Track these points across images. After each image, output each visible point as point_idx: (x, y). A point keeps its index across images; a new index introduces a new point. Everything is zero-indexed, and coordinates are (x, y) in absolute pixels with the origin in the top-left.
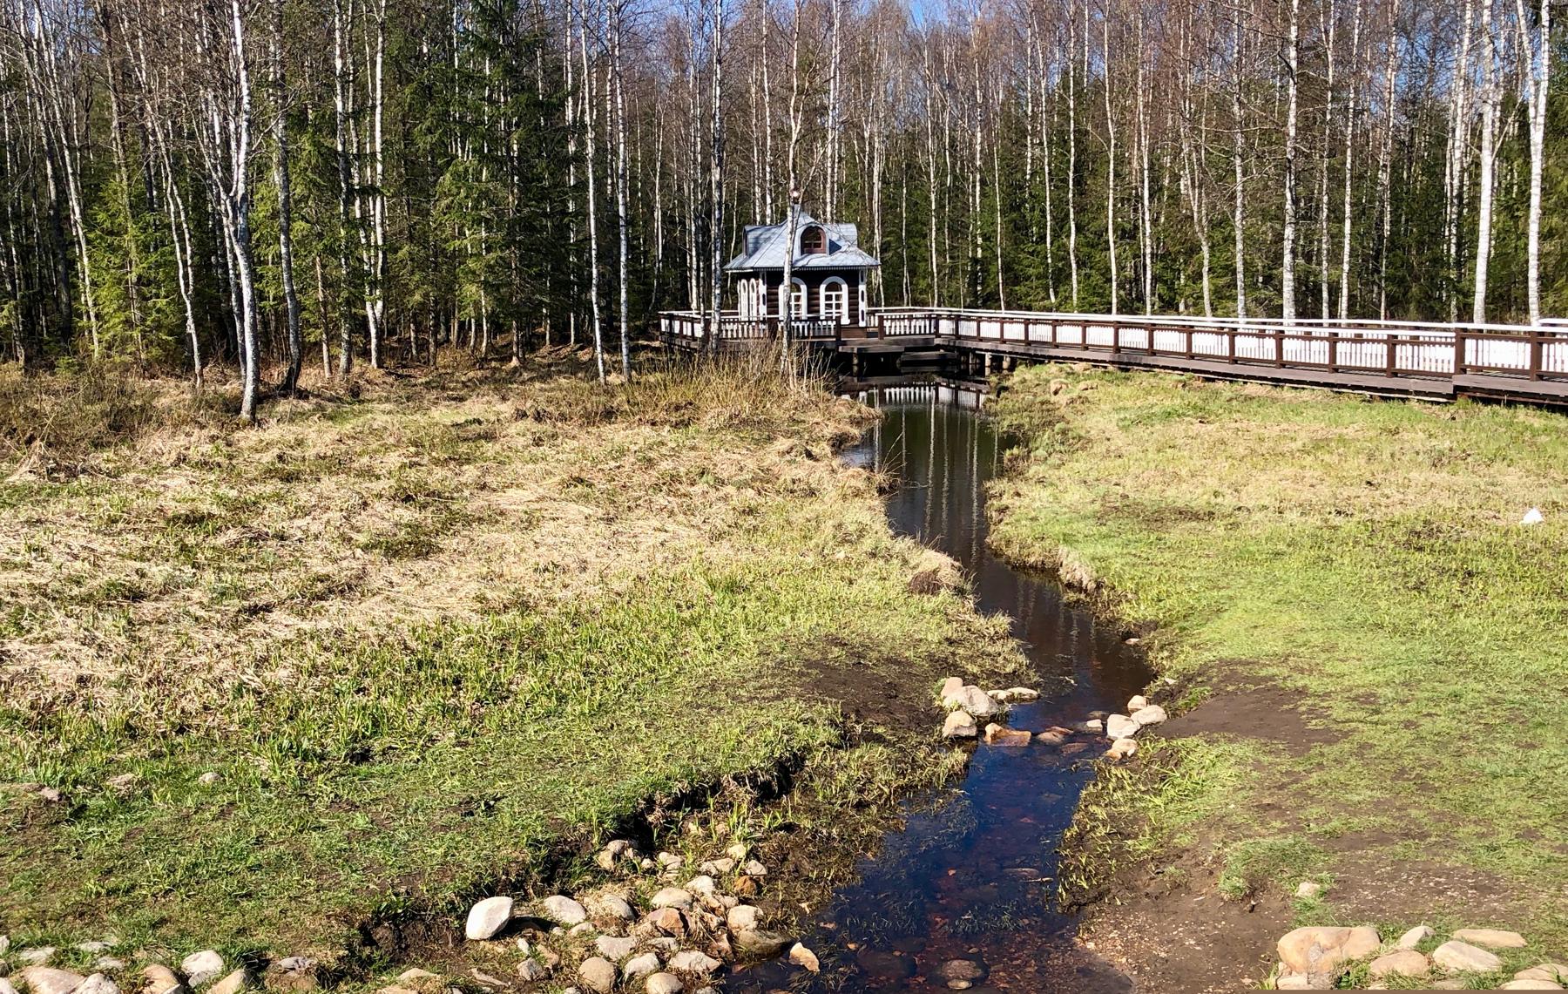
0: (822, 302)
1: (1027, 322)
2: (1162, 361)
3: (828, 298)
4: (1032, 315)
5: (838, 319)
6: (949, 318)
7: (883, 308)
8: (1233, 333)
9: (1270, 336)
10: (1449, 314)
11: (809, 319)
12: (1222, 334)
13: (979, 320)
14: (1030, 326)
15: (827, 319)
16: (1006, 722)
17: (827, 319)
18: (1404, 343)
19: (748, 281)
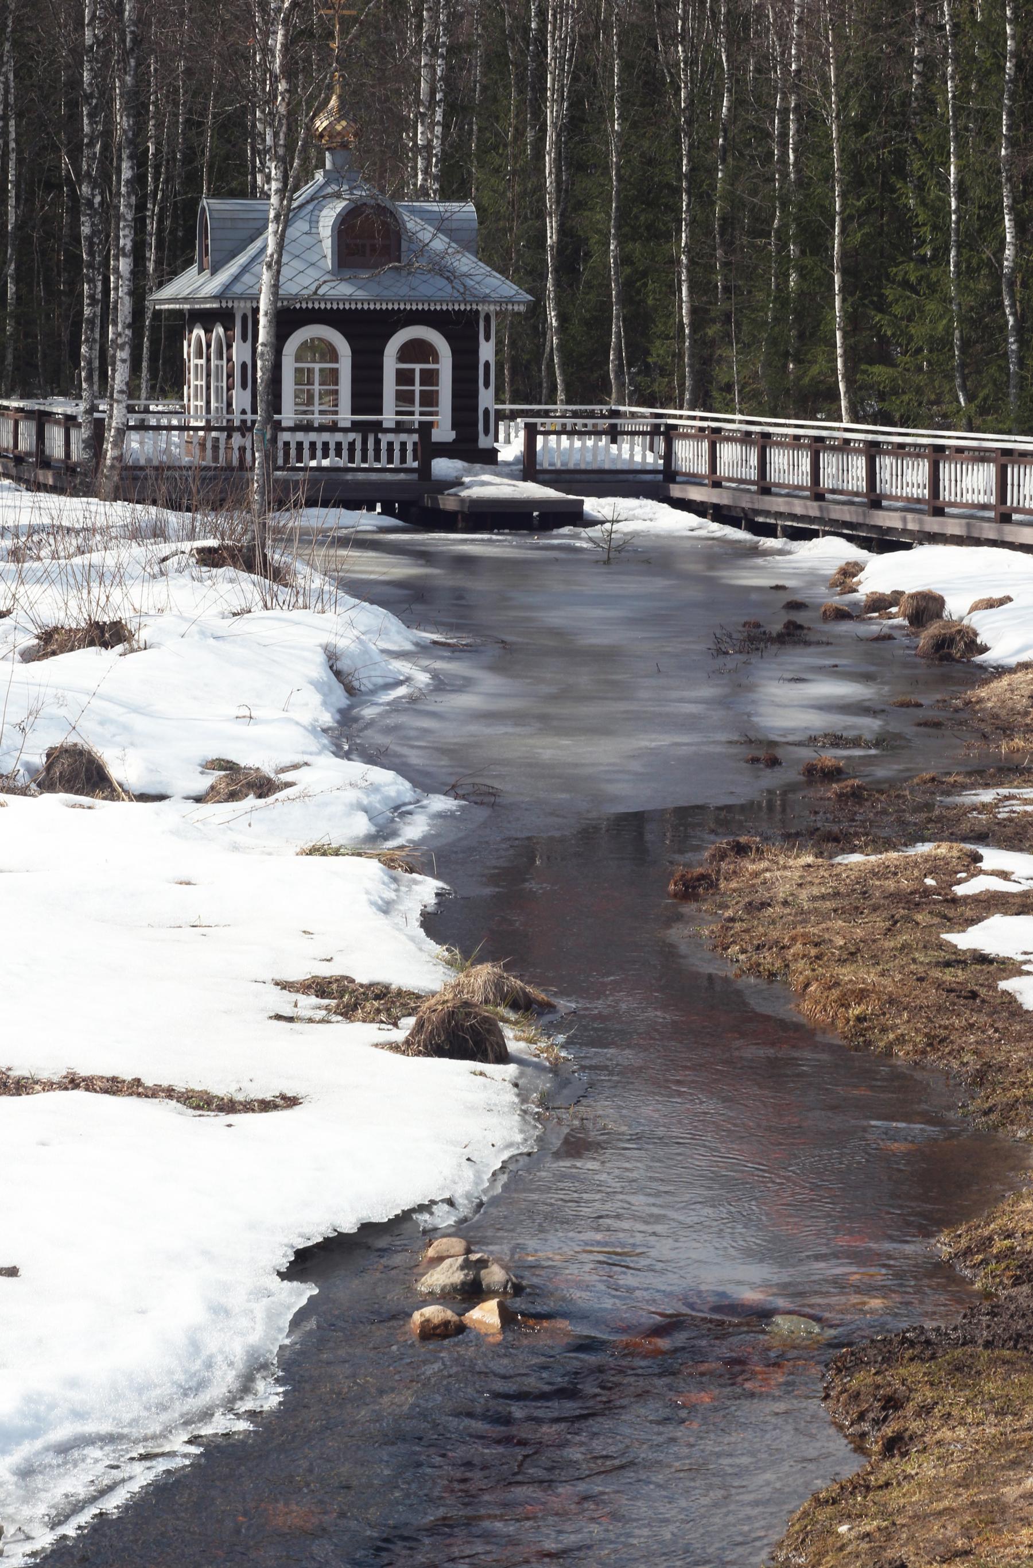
0: (389, 386)
1: (873, 451)
2: (900, 504)
3: (404, 377)
4: (951, 438)
5: (426, 428)
6: (746, 438)
7: (559, 407)
8: (670, 433)
9: (857, 451)
10: (682, 400)
11: (356, 426)
12: (702, 439)
13: (873, 451)
14: (825, 458)
15: (400, 428)
16: (527, 1009)
17: (400, 428)
18: (686, 436)
19: (208, 331)
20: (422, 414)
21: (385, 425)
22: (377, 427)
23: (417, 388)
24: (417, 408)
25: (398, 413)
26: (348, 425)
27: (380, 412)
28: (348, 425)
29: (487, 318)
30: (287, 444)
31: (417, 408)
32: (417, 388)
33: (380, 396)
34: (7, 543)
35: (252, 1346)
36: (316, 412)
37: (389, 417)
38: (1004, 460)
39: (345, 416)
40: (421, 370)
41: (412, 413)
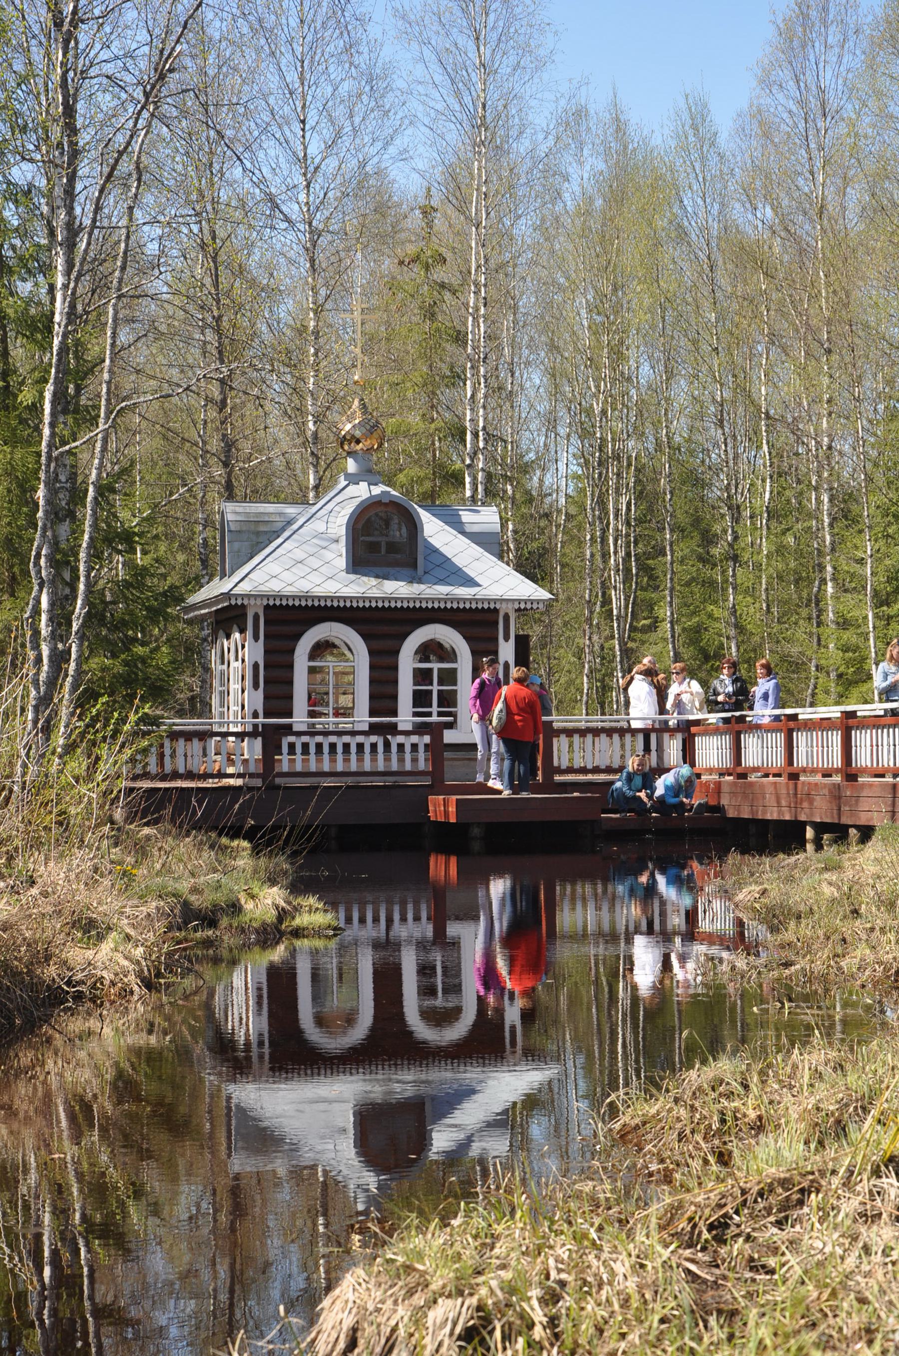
3: (422, 676)
11: (374, 729)
20: (440, 714)
21: (296, 728)
22: (393, 729)
23: (435, 688)
24: (435, 709)
25: (416, 714)
26: (366, 728)
27: (290, 715)
28: (366, 728)
29: (507, 618)
30: (401, 746)
31: (435, 709)
32: (435, 688)
33: (394, 697)
34: (59, 1353)
35: (526, 1095)
36: (435, 714)
37: (405, 717)
38: (738, 727)
39: (362, 718)
40: (439, 670)
41: (429, 714)
